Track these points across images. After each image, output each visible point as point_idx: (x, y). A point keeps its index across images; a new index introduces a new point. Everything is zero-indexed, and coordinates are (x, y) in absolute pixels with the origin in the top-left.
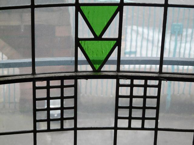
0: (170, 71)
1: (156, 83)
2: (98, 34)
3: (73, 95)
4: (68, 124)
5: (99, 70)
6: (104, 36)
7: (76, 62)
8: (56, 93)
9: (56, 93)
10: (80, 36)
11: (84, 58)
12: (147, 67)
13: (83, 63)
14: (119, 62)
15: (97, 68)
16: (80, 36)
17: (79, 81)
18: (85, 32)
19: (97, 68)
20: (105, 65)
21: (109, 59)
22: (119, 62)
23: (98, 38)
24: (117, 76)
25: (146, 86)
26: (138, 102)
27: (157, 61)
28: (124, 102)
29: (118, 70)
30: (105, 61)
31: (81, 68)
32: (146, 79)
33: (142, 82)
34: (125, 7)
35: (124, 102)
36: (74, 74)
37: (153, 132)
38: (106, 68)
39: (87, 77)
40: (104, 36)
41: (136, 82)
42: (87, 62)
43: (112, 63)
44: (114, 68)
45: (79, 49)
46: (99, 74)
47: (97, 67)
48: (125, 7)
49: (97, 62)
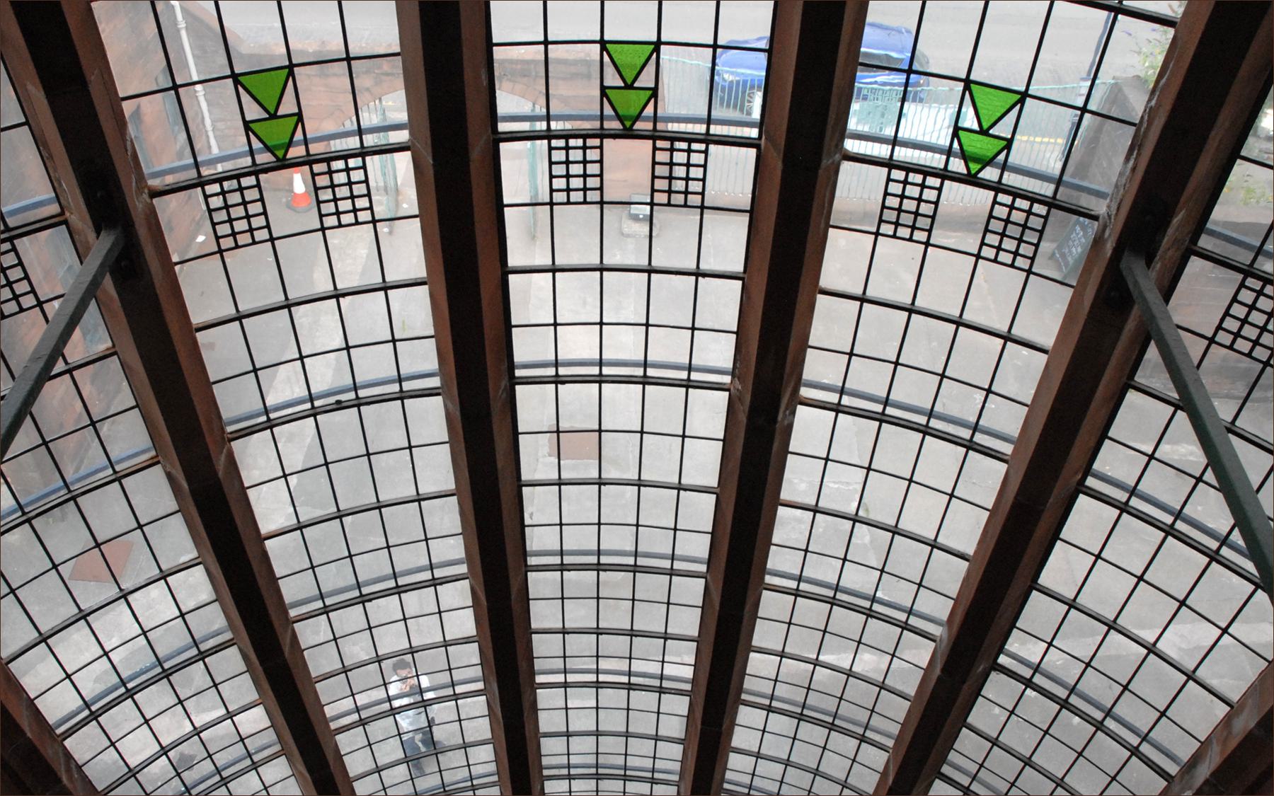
0: (718, 133)
1: (702, 147)
2: (629, 82)
3: (935, 200)
4: (593, 196)
5: (631, 128)
6: (636, 85)
7: (252, 152)
8: (576, 155)
9: (576, 155)
10: (606, 84)
11: (612, 113)
12: (690, 128)
13: (610, 118)
14: (306, 142)
15: (628, 126)
16: (606, 84)
17: (605, 140)
18: (612, 79)
19: (628, 126)
20: (637, 123)
21: (643, 114)
22: (655, 119)
23: (629, 86)
24: (654, 136)
25: (584, 148)
26: (909, 205)
27: (703, 119)
28: (893, 202)
29: (655, 129)
30: (638, 117)
31: (607, 125)
32: (690, 141)
33: (580, 142)
34: (662, 47)
35: (893, 202)
36: (599, 132)
37: (582, 179)
38: (639, 125)
39: (615, 136)
40: (636, 85)
41: (572, 142)
42: (265, 149)
43: (647, 119)
44: (649, 126)
45: (605, 99)
46: (630, 133)
47: (628, 124)
48: (662, 47)
49: (279, 147)
